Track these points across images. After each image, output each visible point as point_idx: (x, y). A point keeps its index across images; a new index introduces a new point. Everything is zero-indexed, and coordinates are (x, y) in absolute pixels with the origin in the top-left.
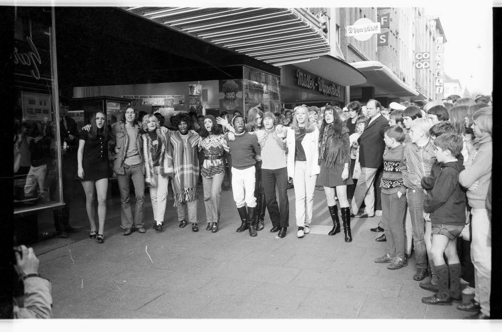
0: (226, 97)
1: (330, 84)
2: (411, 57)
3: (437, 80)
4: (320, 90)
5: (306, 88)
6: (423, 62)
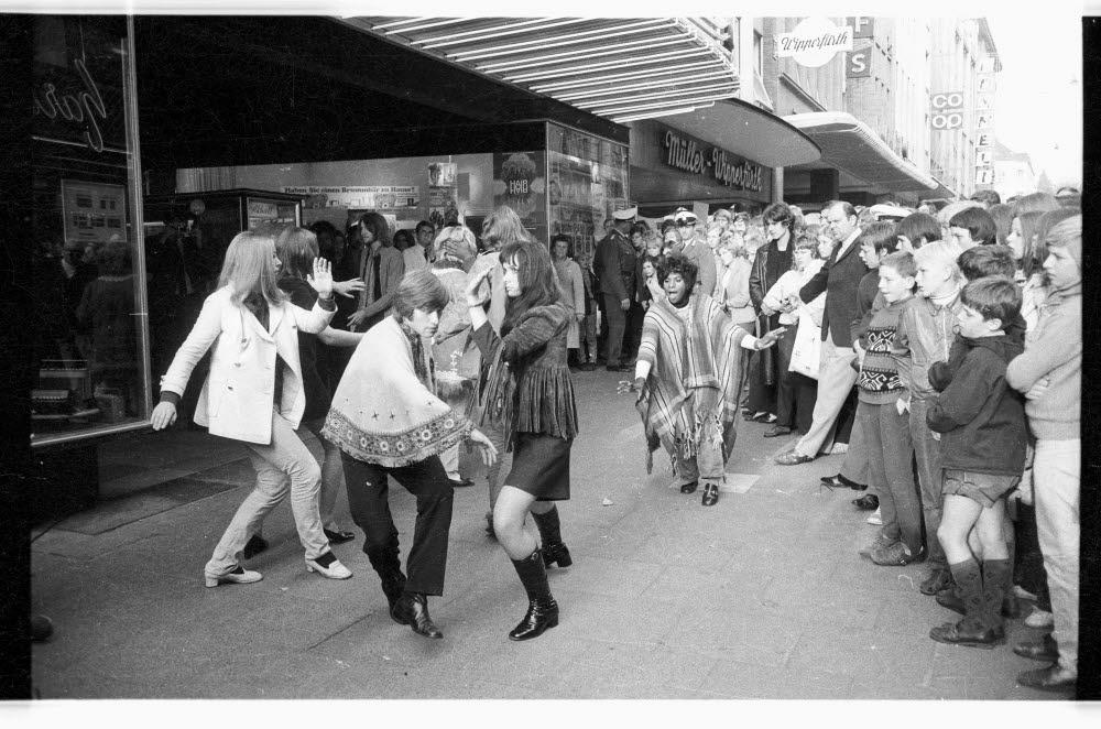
0: (508, 190)
1: (740, 162)
2: (923, 106)
3: (980, 154)
4: (718, 175)
5: (685, 171)
6: (947, 116)
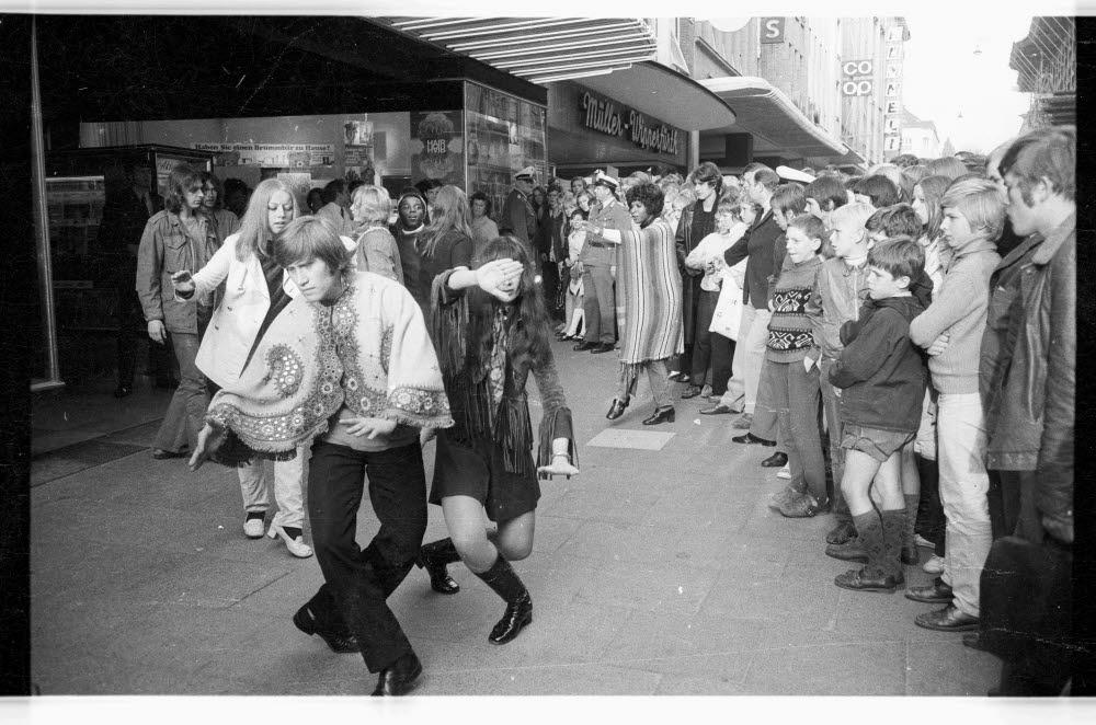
0: (425, 149)
1: (656, 125)
2: (833, 71)
3: (888, 122)
6: (857, 83)
